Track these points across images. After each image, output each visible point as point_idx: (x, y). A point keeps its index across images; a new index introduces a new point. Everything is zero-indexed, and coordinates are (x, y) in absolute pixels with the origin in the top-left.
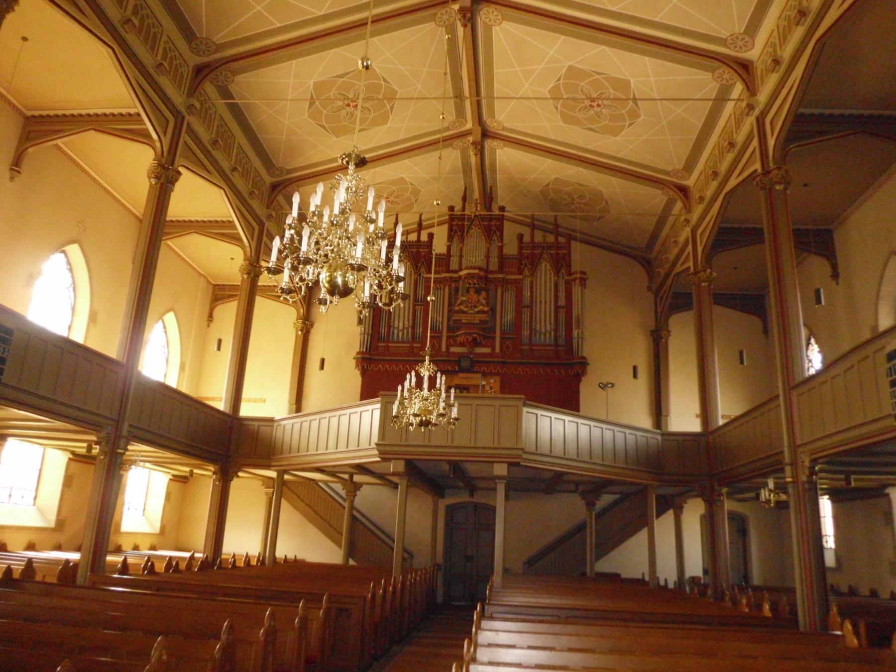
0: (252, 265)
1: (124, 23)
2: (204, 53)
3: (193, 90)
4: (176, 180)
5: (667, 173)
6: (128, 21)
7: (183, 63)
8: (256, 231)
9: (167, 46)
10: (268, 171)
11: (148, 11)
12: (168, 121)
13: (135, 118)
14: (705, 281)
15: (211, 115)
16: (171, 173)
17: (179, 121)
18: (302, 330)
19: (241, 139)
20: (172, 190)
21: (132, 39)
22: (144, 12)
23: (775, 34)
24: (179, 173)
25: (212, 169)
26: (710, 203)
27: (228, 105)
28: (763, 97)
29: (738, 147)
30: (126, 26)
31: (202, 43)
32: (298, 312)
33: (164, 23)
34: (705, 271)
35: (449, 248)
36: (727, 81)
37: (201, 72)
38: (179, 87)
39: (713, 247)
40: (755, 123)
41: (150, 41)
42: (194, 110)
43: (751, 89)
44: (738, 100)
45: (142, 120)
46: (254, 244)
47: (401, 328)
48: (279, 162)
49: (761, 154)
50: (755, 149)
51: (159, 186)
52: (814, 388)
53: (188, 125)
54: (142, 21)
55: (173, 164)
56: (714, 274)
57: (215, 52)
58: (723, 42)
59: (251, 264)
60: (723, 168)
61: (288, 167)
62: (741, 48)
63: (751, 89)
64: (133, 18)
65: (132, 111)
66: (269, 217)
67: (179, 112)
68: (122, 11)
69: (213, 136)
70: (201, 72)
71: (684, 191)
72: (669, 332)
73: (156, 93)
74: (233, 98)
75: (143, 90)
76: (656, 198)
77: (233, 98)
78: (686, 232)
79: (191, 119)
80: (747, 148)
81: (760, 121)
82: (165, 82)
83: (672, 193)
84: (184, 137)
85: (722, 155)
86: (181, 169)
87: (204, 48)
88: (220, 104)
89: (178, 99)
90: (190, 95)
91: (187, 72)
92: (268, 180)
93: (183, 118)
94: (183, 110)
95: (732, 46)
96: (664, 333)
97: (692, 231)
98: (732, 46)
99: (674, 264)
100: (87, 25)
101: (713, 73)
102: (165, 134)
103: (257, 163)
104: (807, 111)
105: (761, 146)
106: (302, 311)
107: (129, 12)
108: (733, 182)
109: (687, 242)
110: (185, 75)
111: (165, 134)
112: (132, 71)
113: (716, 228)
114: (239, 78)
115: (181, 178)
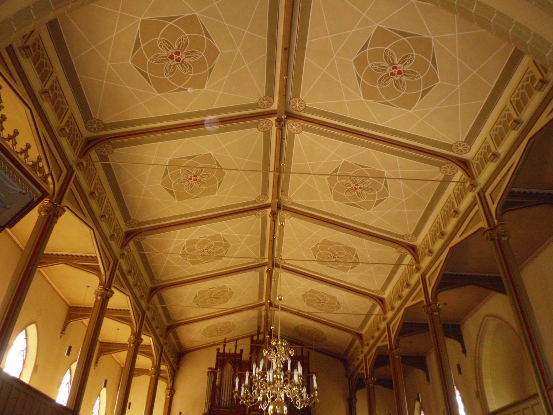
0: (106, 290)
1: (43, 93)
2: (95, 129)
3: (84, 153)
4: (61, 215)
5: (353, 328)
6: (136, 285)
7: (93, 168)
8: (141, 316)
9: (54, 84)
10: (126, 222)
11: (103, 191)
12: (62, 172)
13: (94, 259)
14: (397, 355)
15: (92, 174)
16: (109, 293)
17: (70, 172)
18: (134, 343)
19: (110, 195)
20: (56, 222)
21: (47, 106)
22: (99, 186)
23: (440, 216)
24: (113, 292)
25: (127, 287)
26: (405, 300)
27: (140, 254)
28: (482, 179)
29: (412, 286)
30: (43, 96)
31: (95, 122)
32: (133, 330)
33: (116, 212)
34: (396, 349)
35: (251, 358)
36: (450, 173)
37: (90, 143)
38: (74, 149)
39: (504, 207)
40: (420, 277)
41: (74, 144)
42: (81, 166)
43: (417, 260)
44: (377, 315)
45: (97, 261)
46: (108, 274)
47: (225, 400)
48: (96, 115)
49: (424, 291)
50: (421, 289)
51: (47, 217)
52: (518, 411)
53: (76, 177)
54: (71, 130)
55: (60, 203)
56: (401, 350)
57: (103, 129)
58: (373, 291)
59: (136, 338)
60: (449, 229)
61: (140, 220)
62: (462, 151)
63: (417, 260)
64: (66, 128)
65: (93, 255)
66: (122, 255)
67: (71, 167)
68: (43, 86)
69: (92, 189)
70: (129, 235)
71: (381, 301)
72: (356, 399)
73: (76, 188)
74: (143, 251)
75: (50, 150)
76: (349, 337)
77: (143, 251)
78: (361, 356)
79: (79, 174)
80: (433, 265)
81: (423, 277)
82: (64, 142)
83: (374, 301)
84: (71, 186)
85: (434, 241)
86: (114, 289)
87: (95, 126)
88: (99, 166)
89: (71, 156)
90: (148, 302)
91: (122, 235)
92: (125, 229)
93: (73, 172)
94: (145, 309)
95: (456, 150)
96: (353, 401)
97: (387, 324)
98: (456, 150)
99: (354, 372)
100: (15, 88)
101: (440, 167)
102: (58, 180)
103: (118, 215)
104: (516, 190)
105: (424, 287)
106: (170, 385)
107: (48, 87)
108: (456, 240)
109: (362, 361)
110: (79, 143)
111: (58, 180)
112: (42, 129)
113: (441, 275)
114: (116, 151)
115: (114, 295)
